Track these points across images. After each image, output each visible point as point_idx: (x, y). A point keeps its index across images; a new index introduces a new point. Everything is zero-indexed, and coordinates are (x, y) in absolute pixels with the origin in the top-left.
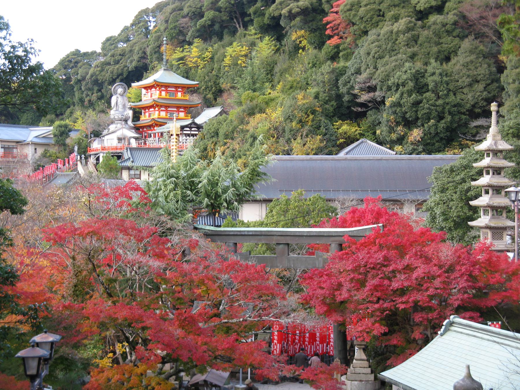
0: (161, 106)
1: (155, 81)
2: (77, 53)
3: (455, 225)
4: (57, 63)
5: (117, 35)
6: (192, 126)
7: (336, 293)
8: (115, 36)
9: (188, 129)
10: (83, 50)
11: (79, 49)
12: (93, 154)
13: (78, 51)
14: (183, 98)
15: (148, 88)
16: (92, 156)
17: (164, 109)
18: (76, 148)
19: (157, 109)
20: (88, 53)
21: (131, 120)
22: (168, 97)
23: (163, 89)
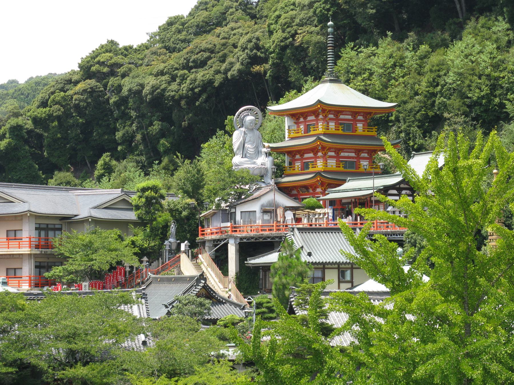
0: (330, 149)
1: (319, 102)
2: (111, 46)
3: (318, 152)
4: (165, 23)
5: (121, 46)
6: (402, 186)
7: (103, 89)
8: (183, 17)
9: (395, 192)
10: (122, 43)
11: (116, 39)
12: (210, 241)
13: (112, 43)
14: (366, 133)
15: (297, 115)
16: (207, 244)
17: (333, 154)
18: (173, 228)
19: (320, 154)
20: (131, 47)
21: (270, 174)
22: (340, 132)
23: (331, 116)
